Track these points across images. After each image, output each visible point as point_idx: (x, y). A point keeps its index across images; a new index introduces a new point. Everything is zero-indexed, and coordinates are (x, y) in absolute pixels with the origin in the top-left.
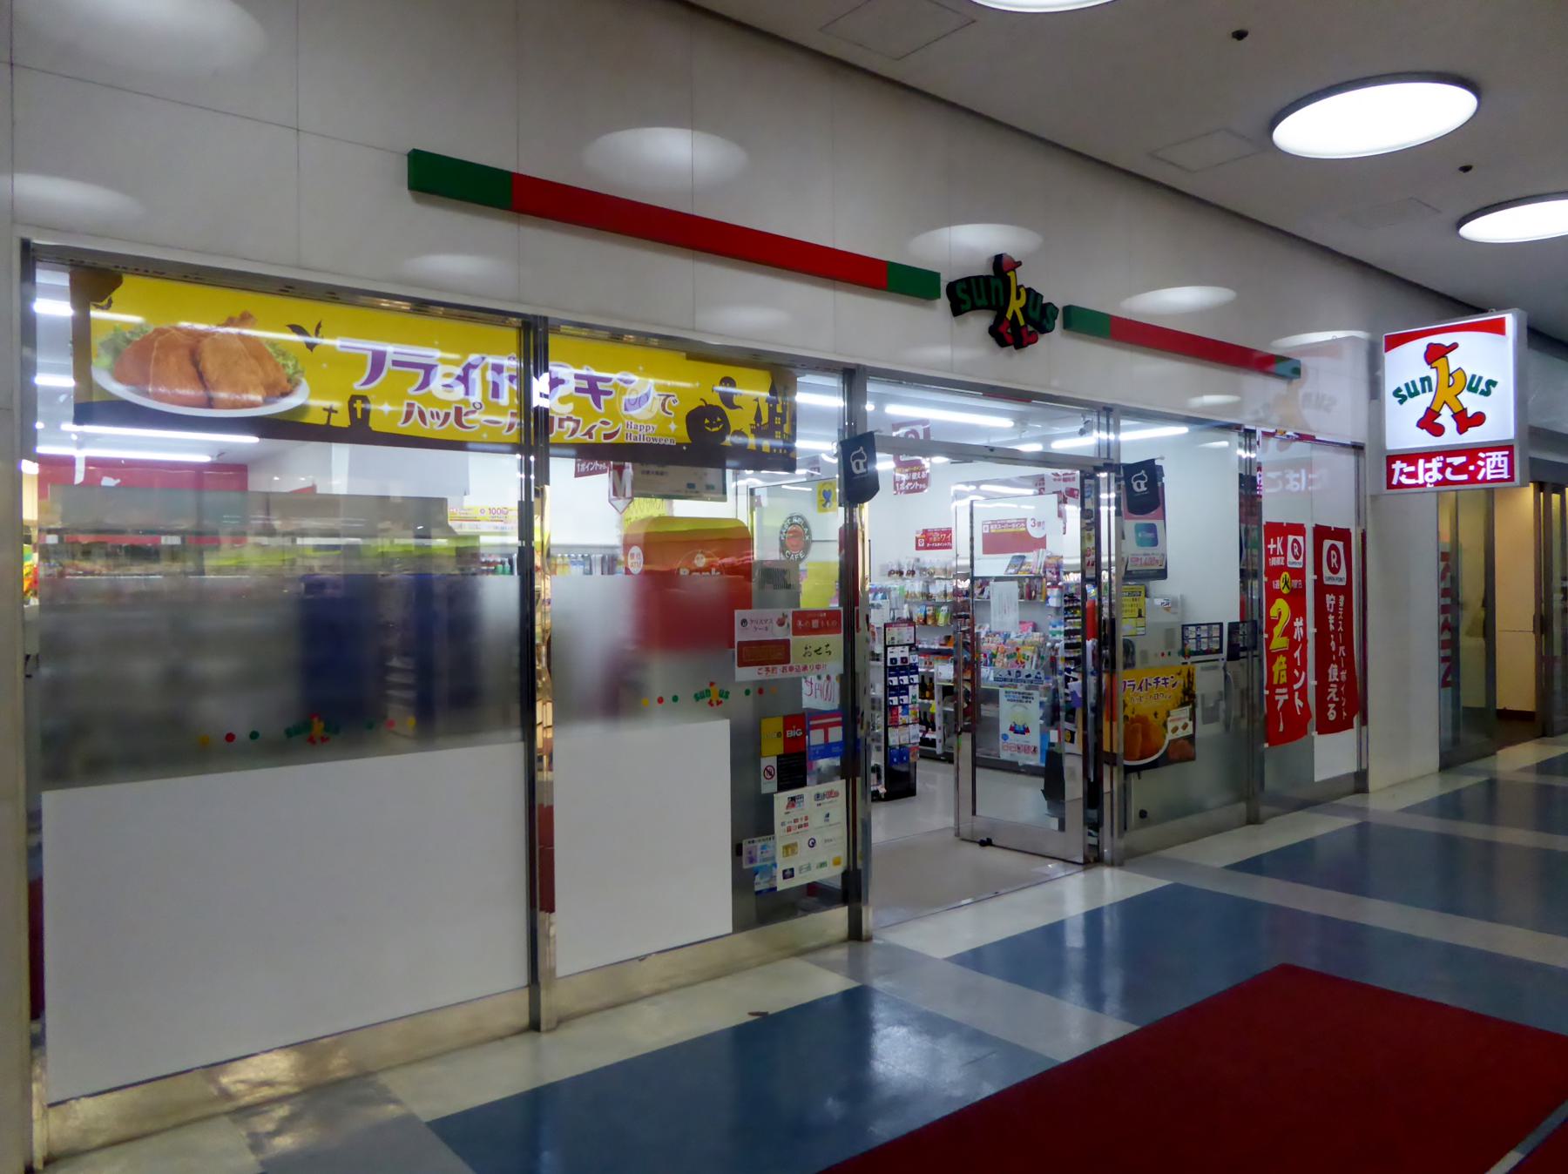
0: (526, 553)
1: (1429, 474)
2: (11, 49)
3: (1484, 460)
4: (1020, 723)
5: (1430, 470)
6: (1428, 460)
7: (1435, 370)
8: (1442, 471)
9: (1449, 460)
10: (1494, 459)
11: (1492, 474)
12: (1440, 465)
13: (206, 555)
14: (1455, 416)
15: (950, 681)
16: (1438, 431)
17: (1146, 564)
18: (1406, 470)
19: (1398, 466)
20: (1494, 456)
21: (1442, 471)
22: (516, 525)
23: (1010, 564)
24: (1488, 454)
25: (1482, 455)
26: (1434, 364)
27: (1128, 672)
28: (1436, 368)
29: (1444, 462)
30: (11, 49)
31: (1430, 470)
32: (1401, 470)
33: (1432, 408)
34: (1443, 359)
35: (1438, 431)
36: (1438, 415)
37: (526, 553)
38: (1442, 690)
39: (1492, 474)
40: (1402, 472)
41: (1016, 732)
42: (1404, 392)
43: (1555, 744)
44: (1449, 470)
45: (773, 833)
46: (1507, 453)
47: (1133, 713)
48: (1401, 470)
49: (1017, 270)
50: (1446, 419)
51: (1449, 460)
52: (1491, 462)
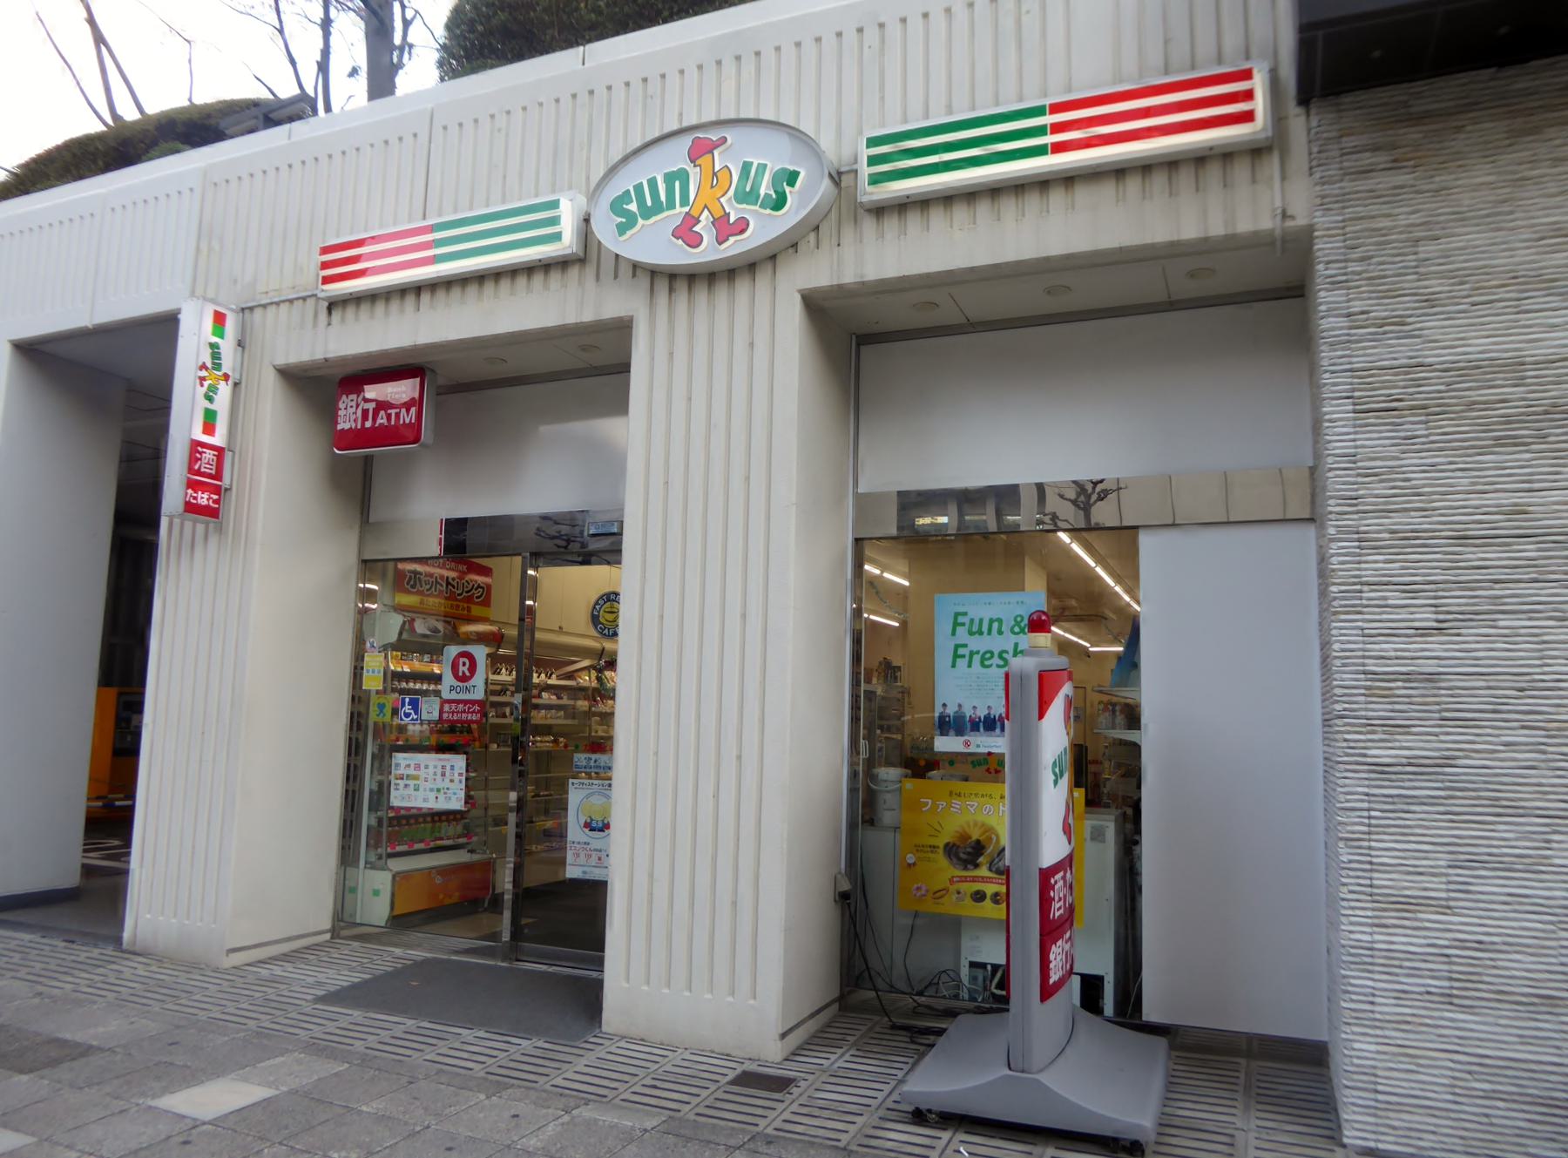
0: (313, 1127)
16: (694, 241)
17: (661, 1113)
23: (903, 727)
24: (204, 450)
25: (200, 449)
26: (698, 162)
28: (700, 166)
33: (691, 213)
36: (698, 221)
37: (313, 1127)
40: (191, 496)
42: (633, 207)
44: (211, 501)
46: (216, 453)
50: (704, 227)
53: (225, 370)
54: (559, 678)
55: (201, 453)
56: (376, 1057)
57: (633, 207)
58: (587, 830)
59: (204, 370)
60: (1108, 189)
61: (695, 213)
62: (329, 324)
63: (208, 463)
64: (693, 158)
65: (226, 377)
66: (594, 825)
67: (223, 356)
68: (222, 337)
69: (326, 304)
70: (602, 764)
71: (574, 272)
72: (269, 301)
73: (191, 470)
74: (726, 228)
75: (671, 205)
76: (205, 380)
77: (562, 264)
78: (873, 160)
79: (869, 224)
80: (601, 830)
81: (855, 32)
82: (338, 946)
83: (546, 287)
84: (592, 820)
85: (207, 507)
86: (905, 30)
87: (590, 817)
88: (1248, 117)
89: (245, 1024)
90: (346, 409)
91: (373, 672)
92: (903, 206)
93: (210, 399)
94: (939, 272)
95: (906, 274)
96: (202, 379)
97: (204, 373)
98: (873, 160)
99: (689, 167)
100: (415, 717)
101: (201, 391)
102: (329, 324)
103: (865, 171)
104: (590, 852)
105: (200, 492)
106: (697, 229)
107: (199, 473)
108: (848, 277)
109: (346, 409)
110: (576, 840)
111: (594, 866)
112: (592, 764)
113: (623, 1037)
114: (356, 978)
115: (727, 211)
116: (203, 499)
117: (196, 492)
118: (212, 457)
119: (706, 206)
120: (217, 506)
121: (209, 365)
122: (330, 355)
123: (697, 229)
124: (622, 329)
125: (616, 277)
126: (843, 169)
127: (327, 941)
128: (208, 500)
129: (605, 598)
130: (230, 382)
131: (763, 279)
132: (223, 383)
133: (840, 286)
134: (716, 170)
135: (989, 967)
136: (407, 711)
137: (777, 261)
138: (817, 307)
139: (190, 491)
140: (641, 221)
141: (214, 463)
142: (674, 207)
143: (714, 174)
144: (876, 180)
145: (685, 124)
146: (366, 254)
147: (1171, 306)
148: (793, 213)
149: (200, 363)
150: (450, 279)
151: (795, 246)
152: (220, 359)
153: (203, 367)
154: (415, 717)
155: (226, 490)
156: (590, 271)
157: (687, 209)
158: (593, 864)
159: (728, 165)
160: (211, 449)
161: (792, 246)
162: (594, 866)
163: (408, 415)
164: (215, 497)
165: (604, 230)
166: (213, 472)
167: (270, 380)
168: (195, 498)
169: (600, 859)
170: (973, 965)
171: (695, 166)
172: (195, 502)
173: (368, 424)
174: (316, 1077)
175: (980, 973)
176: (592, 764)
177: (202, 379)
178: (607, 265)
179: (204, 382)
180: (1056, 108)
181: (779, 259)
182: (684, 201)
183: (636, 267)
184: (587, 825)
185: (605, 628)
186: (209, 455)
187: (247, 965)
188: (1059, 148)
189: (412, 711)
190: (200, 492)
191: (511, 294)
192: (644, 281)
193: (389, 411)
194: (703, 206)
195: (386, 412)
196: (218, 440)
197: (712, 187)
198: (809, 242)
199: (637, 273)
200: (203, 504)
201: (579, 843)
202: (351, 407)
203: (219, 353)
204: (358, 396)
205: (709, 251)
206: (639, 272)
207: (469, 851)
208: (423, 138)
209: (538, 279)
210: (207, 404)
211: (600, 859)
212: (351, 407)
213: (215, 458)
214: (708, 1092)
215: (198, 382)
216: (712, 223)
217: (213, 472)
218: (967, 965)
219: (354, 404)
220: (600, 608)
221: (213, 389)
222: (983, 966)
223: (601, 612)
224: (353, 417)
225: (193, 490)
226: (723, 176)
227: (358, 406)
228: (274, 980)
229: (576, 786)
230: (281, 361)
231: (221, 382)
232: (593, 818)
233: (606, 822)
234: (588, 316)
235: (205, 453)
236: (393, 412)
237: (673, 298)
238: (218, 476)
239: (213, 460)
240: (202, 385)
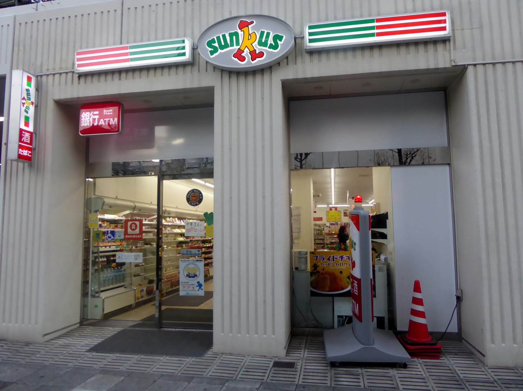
1: (25, 153)
2: (300, 311)
4: (192, 273)
7: (243, 32)
13: (159, 164)
14: (251, 53)
16: (242, 59)
24: (25, 133)
26: (243, 30)
28: (243, 31)
30: (300, 311)
32: (21, 151)
33: (241, 48)
34: (246, 28)
35: (242, 59)
36: (243, 52)
38: (303, 168)
41: (190, 277)
42: (216, 45)
44: (28, 154)
46: (30, 134)
47: (323, 270)
48: (21, 151)
50: (246, 53)
53: (32, 100)
54: (149, 221)
55: (24, 134)
56: (132, 372)
57: (216, 45)
58: (187, 278)
59: (24, 100)
60: (394, 50)
61: (242, 49)
62: (79, 84)
63: (27, 138)
64: (240, 28)
65: (32, 103)
66: (190, 275)
67: (31, 94)
68: (30, 86)
69: (78, 76)
70: (193, 253)
71: (189, 68)
72: (50, 73)
73: (20, 140)
74: (254, 55)
75: (232, 45)
76: (25, 104)
77: (184, 65)
78: (310, 34)
79: (307, 57)
80: (194, 277)
81: (49, 20)
82: (84, 328)
83: (320, 61)
84: (189, 274)
85: (27, 156)
86: (57, 22)
87: (189, 273)
88: (444, 29)
89: (43, 363)
90: (85, 118)
91: (94, 221)
92: (319, 52)
93: (27, 112)
94: (317, 77)
95: (322, 76)
96: (24, 104)
97: (24, 101)
98: (310, 34)
99: (239, 31)
100: (113, 238)
101: (23, 108)
102: (79, 84)
103: (307, 37)
104: (189, 286)
105: (24, 150)
106: (243, 54)
107: (23, 142)
108: (300, 76)
109: (85, 118)
110: (183, 281)
111: (191, 291)
112: (189, 253)
113: (223, 354)
114: (99, 340)
115: (244, 51)
116: (25, 153)
117: (23, 150)
118: (28, 136)
119: (246, 46)
120: (30, 156)
121: (26, 98)
122: (121, 93)
123: (243, 54)
124: (210, 91)
125: (207, 71)
126: (297, 37)
127: (78, 327)
128: (27, 153)
129: (192, 191)
130: (34, 105)
131: (267, 76)
132: (31, 105)
133: (297, 79)
134: (250, 34)
135: (344, 317)
136: (109, 236)
137: (272, 69)
138: (286, 85)
139: (20, 150)
140: (220, 51)
141: (29, 138)
142: (233, 46)
143: (249, 34)
144: (311, 41)
145: (233, 16)
146: (175, 50)
147: (399, 92)
148: (278, 53)
149: (22, 97)
150: (135, 68)
151: (279, 64)
152: (30, 96)
153: (24, 99)
154: (113, 238)
155: (34, 149)
156: (196, 68)
157: (239, 47)
158: (191, 290)
159: (255, 32)
160: (28, 133)
161: (278, 64)
162: (191, 291)
163: (114, 121)
164: (30, 152)
165: (205, 52)
166: (29, 142)
167: (51, 105)
168: (22, 153)
169: (193, 288)
170: (339, 316)
171: (241, 31)
172: (22, 154)
173: (96, 124)
174: (114, 384)
175: (341, 319)
176: (189, 253)
177: (24, 104)
178: (203, 65)
179: (24, 105)
180: (378, 20)
181: (273, 68)
182: (238, 44)
183: (215, 68)
184: (187, 276)
185: (192, 202)
186: (27, 135)
187: (52, 340)
188: (379, 34)
189: (112, 236)
190: (24, 150)
191: (99, 82)
192: (219, 74)
193: (105, 119)
194: (245, 46)
195: (104, 119)
196: (31, 129)
197: (249, 39)
198: (284, 62)
199: (215, 70)
200: (26, 155)
201: (184, 282)
202: (87, 117)
203: (30, 93)
204: (90, 113)
205: (248, 63)
206: (215, 69)
207: (124, 288)
208: (119, 12)
209: (173, 70)
210: (26, 114)
211: (193, 288)
212: (87, 117)
213: (29, 136)
214: (183, 365)
215: (22, 104)
216: (249, 53)
217: (29, 142)
218: (337, 317)
219: (89, 116)
220: (190, 195)
221: (28, 108)
222: (342, 317)
223: (190, 197)
224: (88, 121)
225: (21, 149)
226: (253, 36)
227: (90, 117)
228: (66, 346)
229: (182, 261)
230: (57, 97)
231: (30, 105)
232: (190, 272)
233: (195, 274)
234: (195, 85)
235: (26, 134)
236: (107, 120)
237: (238, 79)
238: (31, 144)
239: (28, 137)
240: (24, 106)
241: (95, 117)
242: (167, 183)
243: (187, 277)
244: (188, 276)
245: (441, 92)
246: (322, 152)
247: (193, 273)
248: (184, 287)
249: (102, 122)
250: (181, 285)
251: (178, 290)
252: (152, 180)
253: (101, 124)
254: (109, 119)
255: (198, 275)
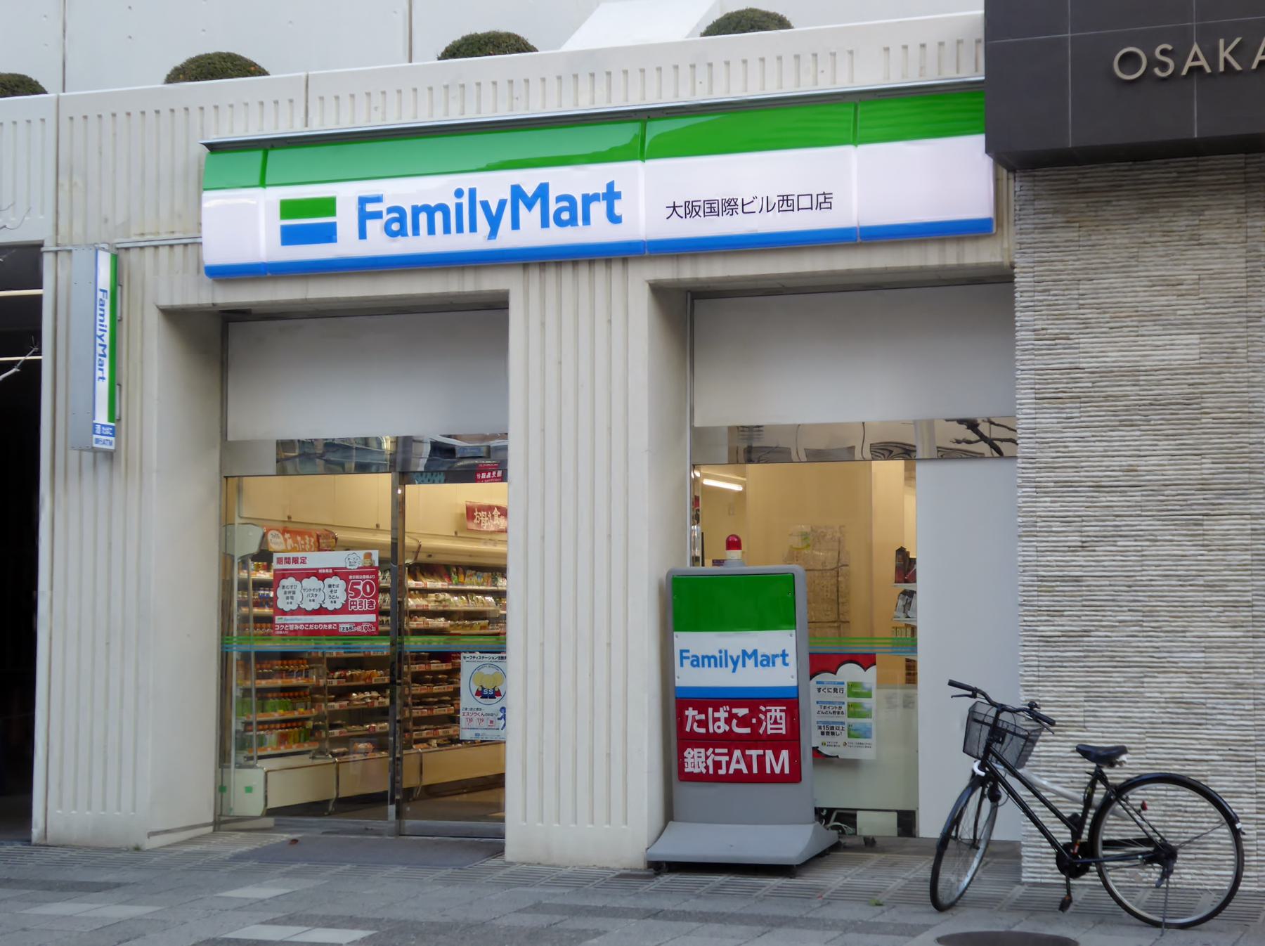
1: (717, 724)
3: (765, 713)
4: (489, 686)
5: (719, 719)
6: (716, 710)
8: (728, 721)
9: (735, 711)
10: (773, 714)
11: (771, 729)
12: (726, 715)
15: (640, 870)
18: (697, 718)
19: (691, 712)
20: (773, 711)
21: (728, 721)
22: (472, 608)
27: (504, 197)
29: (730, 712)
31: (719, 719)
32: (694, 716)
39: (771, 729)
40: (694, 720)
41: (484, 697)
43: (83, 902)
44: (735, 721)
45: (915, 582)
49: (982, 442)
51: (735, 711)
52: (771, 716)
80: (492, 697)
84: (483, 688)
169: (491, 722)
193: (748, 752)
208: (51, 121)
219: (703, 755)
227: (707, 758)
230: (165, 302)
232: (484, 686)
233: (496, 690)
236: (754, 753)
241: (718, 758)
242: (416, 493)
243: (477, 697)
244: (480, 693)
245: (648, 127)
246: (863, 423)
247: (490, 687)
248: (471, 720)
249: (738, 762)
250: (476, 734)
251: (453, 719)
252: (384, 481)
253: (735, 770)
254: (761, 752)
255: (502, 694)
